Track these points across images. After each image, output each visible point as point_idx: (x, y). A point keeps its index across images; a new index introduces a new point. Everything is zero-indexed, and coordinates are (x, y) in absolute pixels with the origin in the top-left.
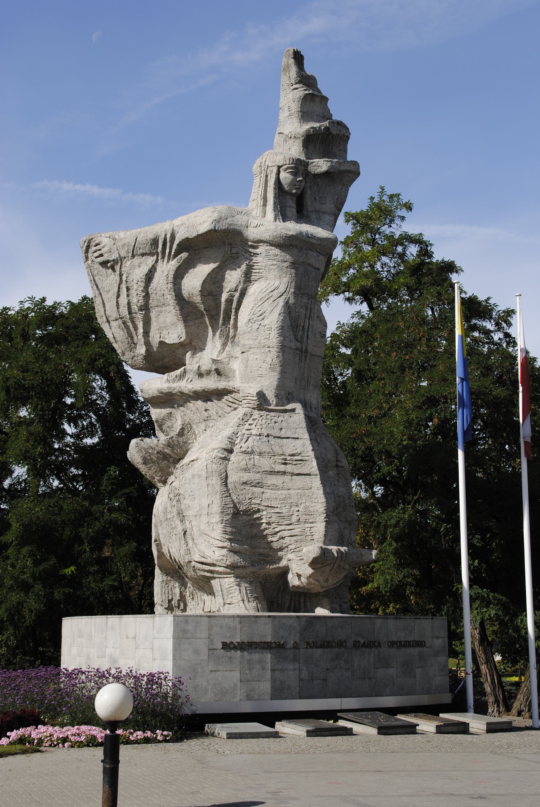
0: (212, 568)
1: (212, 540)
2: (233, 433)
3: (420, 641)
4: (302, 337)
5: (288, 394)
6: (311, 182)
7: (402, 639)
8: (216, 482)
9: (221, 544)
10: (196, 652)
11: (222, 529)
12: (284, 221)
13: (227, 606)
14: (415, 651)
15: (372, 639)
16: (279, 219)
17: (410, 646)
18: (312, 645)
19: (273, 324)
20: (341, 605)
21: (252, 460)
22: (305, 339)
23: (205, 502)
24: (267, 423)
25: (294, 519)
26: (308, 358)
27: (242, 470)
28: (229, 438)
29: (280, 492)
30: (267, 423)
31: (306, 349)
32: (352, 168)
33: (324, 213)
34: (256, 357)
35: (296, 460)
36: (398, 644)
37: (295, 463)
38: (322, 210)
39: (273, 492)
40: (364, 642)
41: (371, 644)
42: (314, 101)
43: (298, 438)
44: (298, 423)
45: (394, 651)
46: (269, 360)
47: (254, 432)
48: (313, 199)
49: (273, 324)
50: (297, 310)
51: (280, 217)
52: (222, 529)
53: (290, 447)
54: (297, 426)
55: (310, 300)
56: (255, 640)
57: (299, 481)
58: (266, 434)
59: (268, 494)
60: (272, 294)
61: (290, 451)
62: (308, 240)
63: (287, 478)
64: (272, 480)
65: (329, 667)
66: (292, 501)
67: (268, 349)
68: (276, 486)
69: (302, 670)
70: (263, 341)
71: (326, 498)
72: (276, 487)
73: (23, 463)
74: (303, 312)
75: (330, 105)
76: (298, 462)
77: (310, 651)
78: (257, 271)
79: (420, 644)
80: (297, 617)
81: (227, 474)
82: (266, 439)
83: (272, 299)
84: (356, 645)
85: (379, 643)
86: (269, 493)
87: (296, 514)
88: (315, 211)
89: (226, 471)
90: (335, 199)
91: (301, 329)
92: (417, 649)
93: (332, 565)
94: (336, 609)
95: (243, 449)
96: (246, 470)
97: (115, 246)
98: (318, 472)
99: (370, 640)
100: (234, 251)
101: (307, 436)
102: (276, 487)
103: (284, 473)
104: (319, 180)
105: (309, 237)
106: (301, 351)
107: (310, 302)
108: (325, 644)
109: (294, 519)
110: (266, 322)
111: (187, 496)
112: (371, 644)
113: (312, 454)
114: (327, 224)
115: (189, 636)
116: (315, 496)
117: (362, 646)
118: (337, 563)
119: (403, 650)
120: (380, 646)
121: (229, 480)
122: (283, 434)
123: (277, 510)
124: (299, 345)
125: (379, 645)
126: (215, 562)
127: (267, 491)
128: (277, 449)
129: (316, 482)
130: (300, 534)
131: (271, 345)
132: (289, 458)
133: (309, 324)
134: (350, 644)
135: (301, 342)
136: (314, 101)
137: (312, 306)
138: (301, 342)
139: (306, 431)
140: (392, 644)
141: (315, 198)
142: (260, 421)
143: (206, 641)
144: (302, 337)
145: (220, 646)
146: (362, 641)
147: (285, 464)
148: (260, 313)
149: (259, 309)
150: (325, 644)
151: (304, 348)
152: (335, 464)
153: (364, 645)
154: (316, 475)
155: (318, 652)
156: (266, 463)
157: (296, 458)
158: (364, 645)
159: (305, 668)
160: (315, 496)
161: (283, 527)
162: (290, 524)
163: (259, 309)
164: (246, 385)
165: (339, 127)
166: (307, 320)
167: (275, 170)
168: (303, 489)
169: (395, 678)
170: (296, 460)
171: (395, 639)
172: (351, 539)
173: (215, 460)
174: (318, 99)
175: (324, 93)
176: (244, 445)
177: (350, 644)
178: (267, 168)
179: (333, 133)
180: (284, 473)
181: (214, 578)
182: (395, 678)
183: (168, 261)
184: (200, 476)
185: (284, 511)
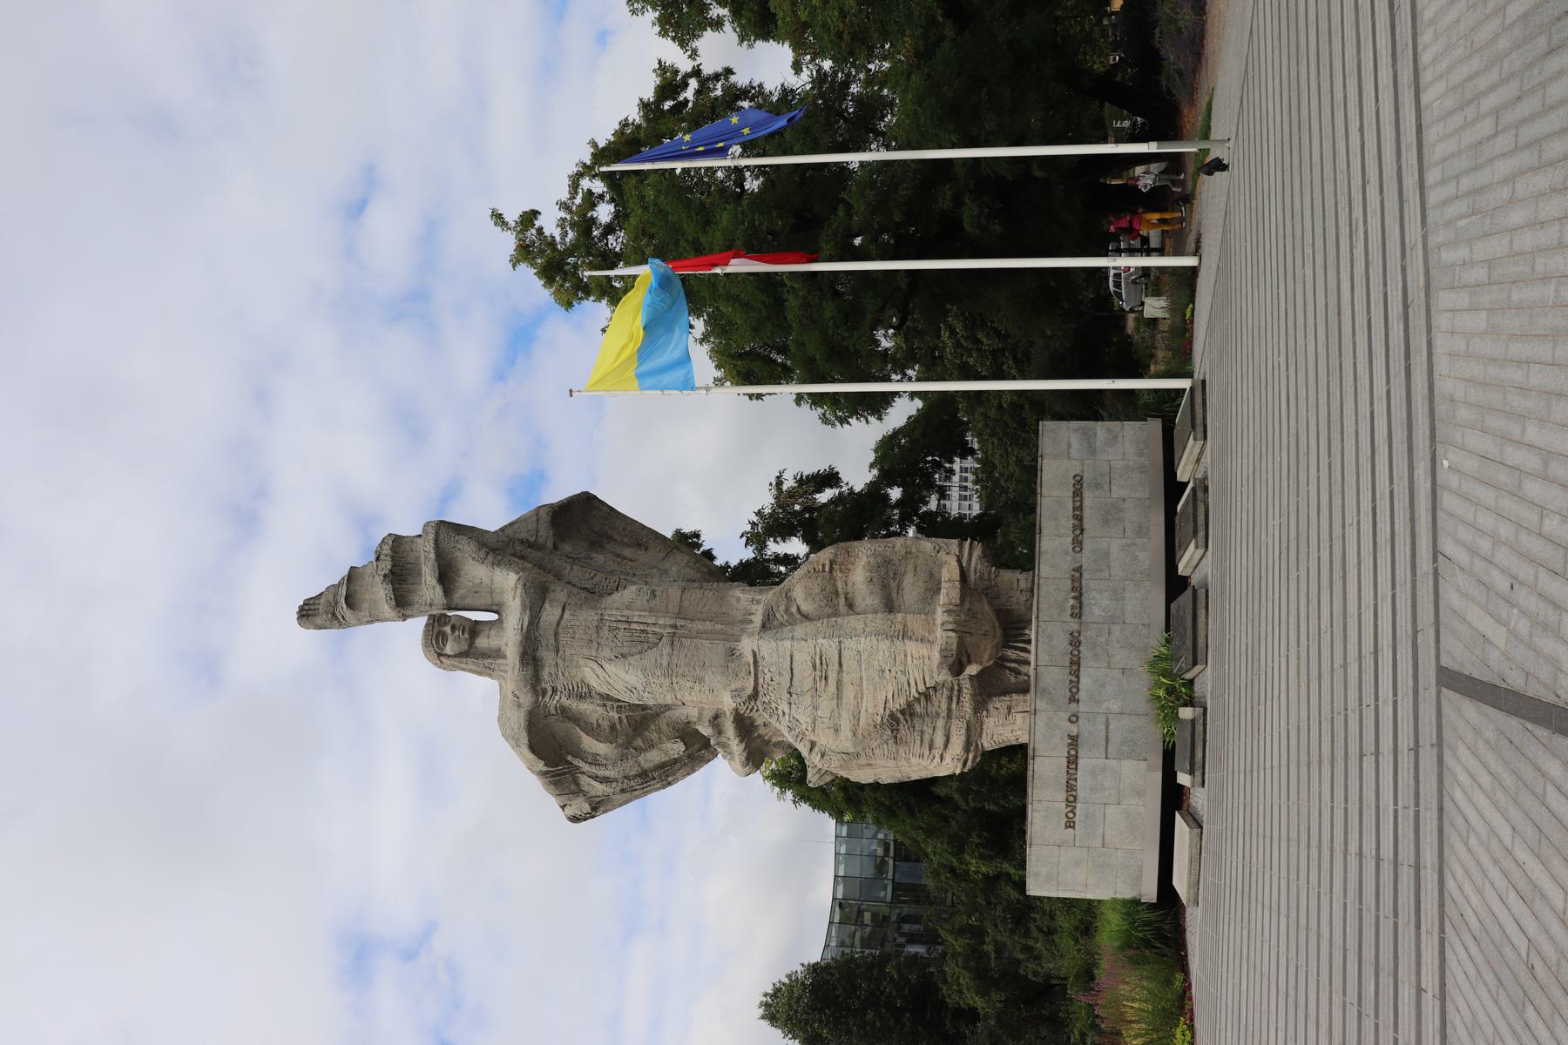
17: (1081, 508)
63: (846, 678)
64: (849, 693)
72: (859, 697)
73: (814, 102)
77: (1082, 695)
79: (1079, 481)
92: (1087, 494)
103: (839, 683)
109: (903, 679)
112: (1078, 592)
119: (1087, 524)
121: (851, 750)
125: (1079, 569)
134: (1074, 625)
140: (1078, 543)
146: (1072, 602)
153: (1079, 598)
155: (1085, 681)
157: (819, 664)
158: (1079, 598)
159: (1105, 705)
168: (859, 662)
177: (1074, 625)
180: (839, 683)
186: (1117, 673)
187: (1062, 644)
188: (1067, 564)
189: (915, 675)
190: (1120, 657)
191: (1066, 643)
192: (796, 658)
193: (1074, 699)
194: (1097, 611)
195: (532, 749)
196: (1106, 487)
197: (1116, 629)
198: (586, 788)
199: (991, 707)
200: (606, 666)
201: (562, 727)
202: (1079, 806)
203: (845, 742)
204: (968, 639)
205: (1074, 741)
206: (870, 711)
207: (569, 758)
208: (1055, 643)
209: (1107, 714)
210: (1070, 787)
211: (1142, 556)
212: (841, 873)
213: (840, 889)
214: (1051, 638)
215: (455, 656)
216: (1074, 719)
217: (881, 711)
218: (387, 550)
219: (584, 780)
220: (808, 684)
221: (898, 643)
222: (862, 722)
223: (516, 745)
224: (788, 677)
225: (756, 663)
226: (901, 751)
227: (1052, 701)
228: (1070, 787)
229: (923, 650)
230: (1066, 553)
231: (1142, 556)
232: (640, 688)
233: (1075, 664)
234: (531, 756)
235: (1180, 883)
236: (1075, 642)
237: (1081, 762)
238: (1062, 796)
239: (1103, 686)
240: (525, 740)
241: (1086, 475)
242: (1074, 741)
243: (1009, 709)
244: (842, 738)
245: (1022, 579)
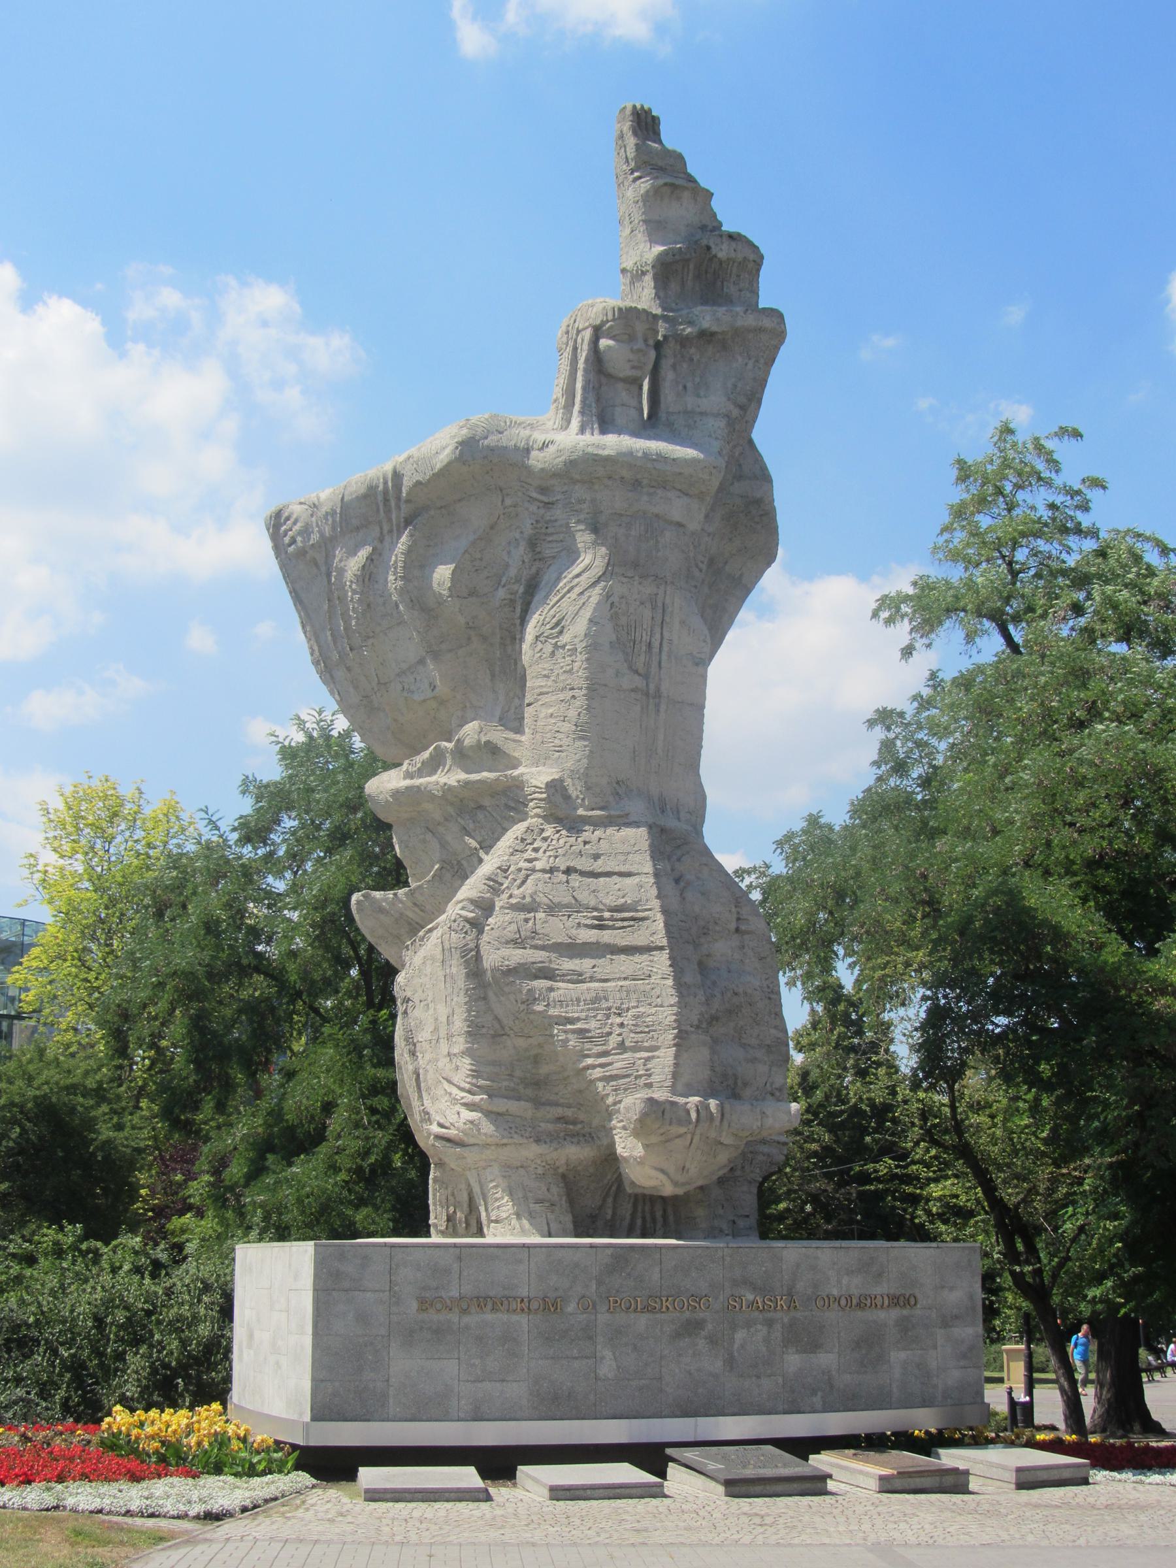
1: (455, 1091)
2: (499, 868)
3: (904, 1296)
4: (648, 665)
5: (618, 783)
6: (675, 356)
8: (457, 969)
9: (469, 1098)
11: (469, 1067)
12: (603, 431)
13: (492, 1225)
16: (592, 429)
19: (577, 640)
20: (734, 1222)
21: (531, 923)
22: (654, 669)
23: (443, 1011)
24: (568, 845)
25: (613, 1041)
26: (663, 707)
27: (507, 942)
28: (489, 879)
29: (585, 986)
30: (568, 845)
31: (658, 690)
32: (767, 323)
34: (550, 711)
35: (623, 920)
36: (843, 1302)
37: (620, 924)
38: (698, 410)
39: (571, 986)
42: (679, 199)
44: (632, 842)
46: (572, 713)
47: (539, 865)
48: (681, 387)
49: (577, 640)
50: (632, 610)
51: (596, 426)
52: (469, 1067)
53: (611, 892)
54: (629, 849)
55: (662, 588)
57: (624, 964)
58: (563, 868)
59: (561, 992)
60: (577, 580)
61: (610, 901)
62: (649, 465)
66: (610, 1004)
67: (571, 693)
68: (581, 975)
69: (603, 1358)
70: (562, 678)
71: (681, 995)
72: (578, 978)
74: (647, 613)
75: (715, 204)
76: (626, 923)
78: (555, 537)
80: (592, 1246)
81: (478, 952)
82: (564, 877)
83: (577, 590)
86: (563, 988)
87: (618, 1031)
88: (686, 412)
89: (477, 946)
90: (729, 385)
91: (644, 648)
92: (895, 1313)
93: (689, 1136)
94: (721, 1231)
95: (513, 901)
96: (518, 942)
97: (314, 519)
98: (664, 942)
100: (508, 502)
101: (648, 867)
102: (578, 978)
104: (693, 350)
105: (654, 460)
106: (647, 694)
107: (661, 592)
109: (613, 1041)
110: (565, 638)
113: (656, 904)
114: (710, 436)
116: (657, 991)
118: (698, 1132)
122: (598, 866)
123: (579, 1025)
124: (639, 682)
127: (561, 984)
128: (584, 897)
129: (661, 962)
130: (623, 1072)
131: (576, 684)
132: (607, 915)
133: (662, 638)
135: (646, 677)
136: (679, 199)
137: (668, 600)
138: (646, 677)
139: (648, 858)
141: (685, 387)
142: (554, 842)
144: (648, 665)
145: (415, 1305)
147: (600, 927)
148: (554, 620)
149: (552, 612)
152: (733, 926)
154: (661, 948)
156: (558, 929)
157: (627, 914)
159: (608, 1354)
160: (657, 991)
161: (590, 1061)
162: (605, 1054)
163: (552, 612)
164: (534, 769)
165: (733, 244)
166: (657, 630)
167: (587, 334)
170: (623, 920)
171: (835, 1292)
172: (772, 1084)
173: (455, 925)
174: (686, 195)
175: (703, 183)
176: (516, 892)
178: (577, 335)
179: (720, 255)
184: (433, 959)
185: (593, 1024)
217: (553, 1012)
221: (670, 1035)
235: (369, 1476)
244: (506, 952)
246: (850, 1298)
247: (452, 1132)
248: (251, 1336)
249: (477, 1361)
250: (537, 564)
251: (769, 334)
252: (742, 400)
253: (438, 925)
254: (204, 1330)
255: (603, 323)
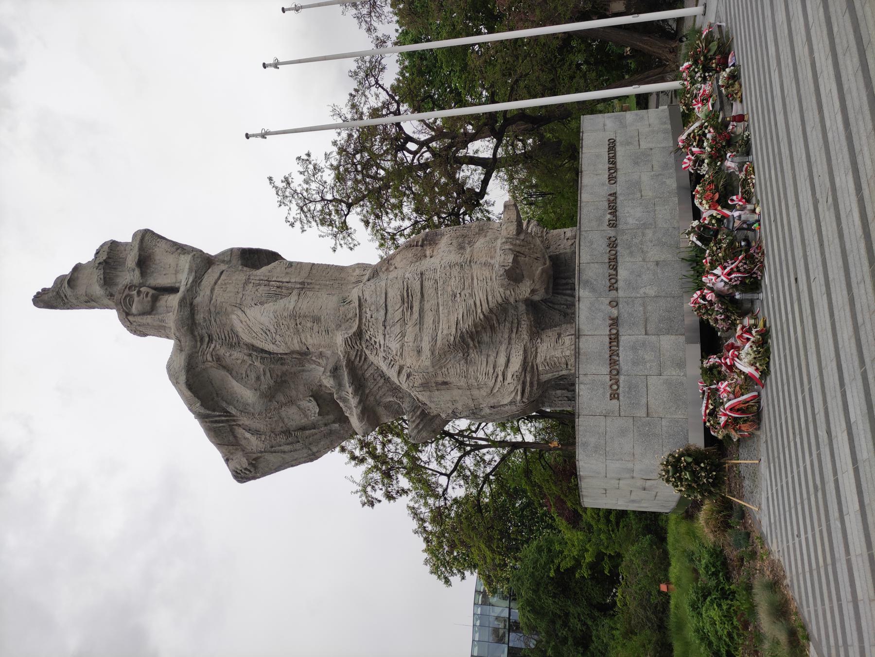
0: (528, 384)
7: (607, 166)
10: (623, 432)
14: (620, 151)
15: (606, 204)
18: (613, 281)
33: (177, 265)
40: (610, 213)
41: (613, 208)
43: (386, 294)
45: (621, 177)
56: (607, 356)
63: (427, 306)
65: (641, 259)
69: (645, 293)
72: (436, 322)
77: (621, 284)
79: (612, 146)
84: (613, 224)
85: (610, 195)
99: (607, 206)
108: (613, 263)
111: (454, 407)
112: (613, 208)
115: (603, 442)
117: (616, 216)
120: (615, 193)
123: (460, 317)
124: (295, 292)
126: (521, 382)
132: (406, 305)
134: (611, 232)
135: (293, 289)
138: (293, 289)
140: (612, 179)
143: (609, 420)
144: (288, 289)
145: (615, 401)
146: (609, 216)
147: (412, 307)
150: (613, 263)
151: (299, 286)
152: (419, 248)
155: (623, 273)
159: (642, 291)
162: (475, 304)
169: (653, 173)
177: (611, 232)
181: (538, 379)
182: (653, 173)
183: (234, 416)
186: (652, 266)
187: (601, 246)
188: (605, 190)
189: (480, 296)
190: (654, 254)
191: (604, 245)
192: (389, 295)
193: (613, 287)
194: (631, 221)
195: (190, 386)
196: (636, 143)
197: (649, 233)
198: (243, 442)
199: (544, 337)
200: (248, 311)
201: (218, 374)
202: (622, 378)
203: (426, 360)
204: (521, 259)
205: (615, 322)
206: (445, 332)
207: (224, 405)
208: (594, 246)
209: (645, 297)
210: (613, 362)
211: (668, 182)
212: (477, 639)
213: (476, 649)
214: (591, 243)
215: (140, 315)
216: (614, 303)
218: (106, 248)
219: (240, 431)
220: (398, 315)
222: (439, 342)
223: (176, 383)
224: (382, 312)
225: (360, 305)
226: (471, 370)
227: (593, 290)
228: (613, 362)
229: (487, 273)
230: (603, 184)
231: (668, 182)
232: (273, 330)
233: (613, 263)
234: (188, 393)
236: (613, 244)
237: (622, 339)
238: (606, 370)
239: (639, 276)
240: (183, 378)
241: (618, 139)
242: (615, 322)
243: (559, 335)
244: (423, 357)
245: (569, 232)
246: (610, 169)
247: (519, 388)
248: (633, 501)
249: (648, 365)
250: (241, 344)
251: (146, 238)
252: (174, 249)
253: (340, 385)
254: (608, 13)
255: (124, 311)
